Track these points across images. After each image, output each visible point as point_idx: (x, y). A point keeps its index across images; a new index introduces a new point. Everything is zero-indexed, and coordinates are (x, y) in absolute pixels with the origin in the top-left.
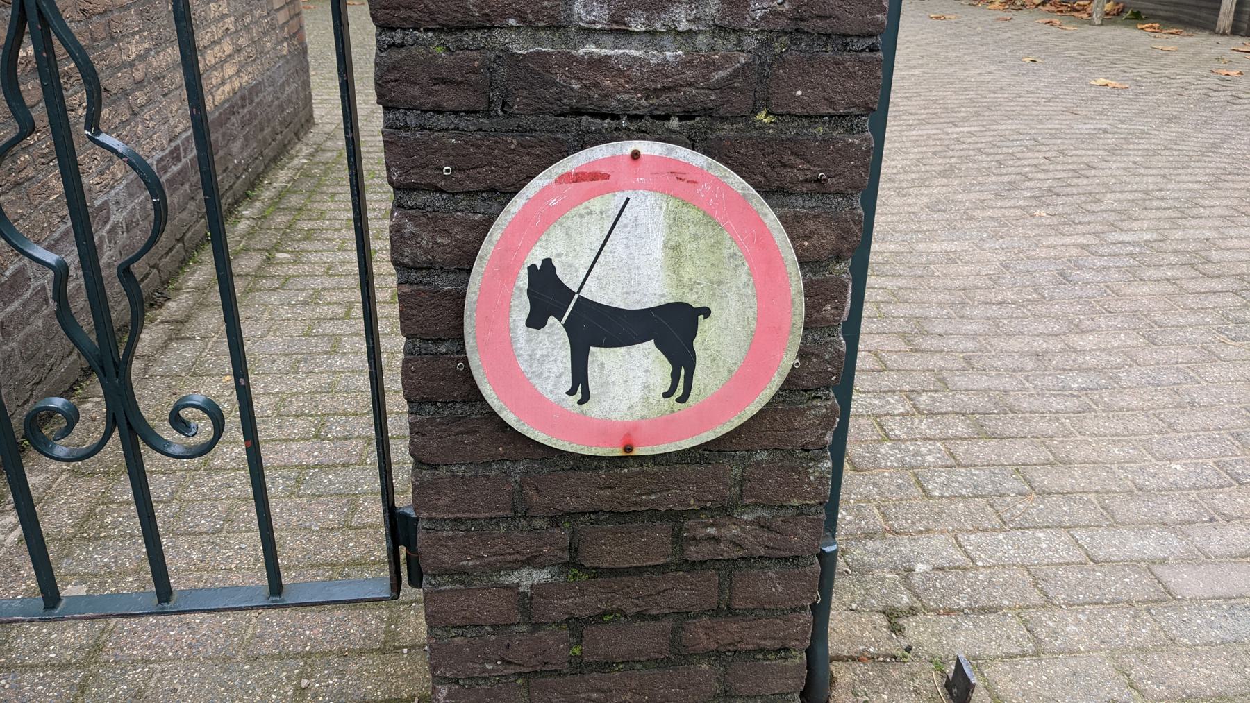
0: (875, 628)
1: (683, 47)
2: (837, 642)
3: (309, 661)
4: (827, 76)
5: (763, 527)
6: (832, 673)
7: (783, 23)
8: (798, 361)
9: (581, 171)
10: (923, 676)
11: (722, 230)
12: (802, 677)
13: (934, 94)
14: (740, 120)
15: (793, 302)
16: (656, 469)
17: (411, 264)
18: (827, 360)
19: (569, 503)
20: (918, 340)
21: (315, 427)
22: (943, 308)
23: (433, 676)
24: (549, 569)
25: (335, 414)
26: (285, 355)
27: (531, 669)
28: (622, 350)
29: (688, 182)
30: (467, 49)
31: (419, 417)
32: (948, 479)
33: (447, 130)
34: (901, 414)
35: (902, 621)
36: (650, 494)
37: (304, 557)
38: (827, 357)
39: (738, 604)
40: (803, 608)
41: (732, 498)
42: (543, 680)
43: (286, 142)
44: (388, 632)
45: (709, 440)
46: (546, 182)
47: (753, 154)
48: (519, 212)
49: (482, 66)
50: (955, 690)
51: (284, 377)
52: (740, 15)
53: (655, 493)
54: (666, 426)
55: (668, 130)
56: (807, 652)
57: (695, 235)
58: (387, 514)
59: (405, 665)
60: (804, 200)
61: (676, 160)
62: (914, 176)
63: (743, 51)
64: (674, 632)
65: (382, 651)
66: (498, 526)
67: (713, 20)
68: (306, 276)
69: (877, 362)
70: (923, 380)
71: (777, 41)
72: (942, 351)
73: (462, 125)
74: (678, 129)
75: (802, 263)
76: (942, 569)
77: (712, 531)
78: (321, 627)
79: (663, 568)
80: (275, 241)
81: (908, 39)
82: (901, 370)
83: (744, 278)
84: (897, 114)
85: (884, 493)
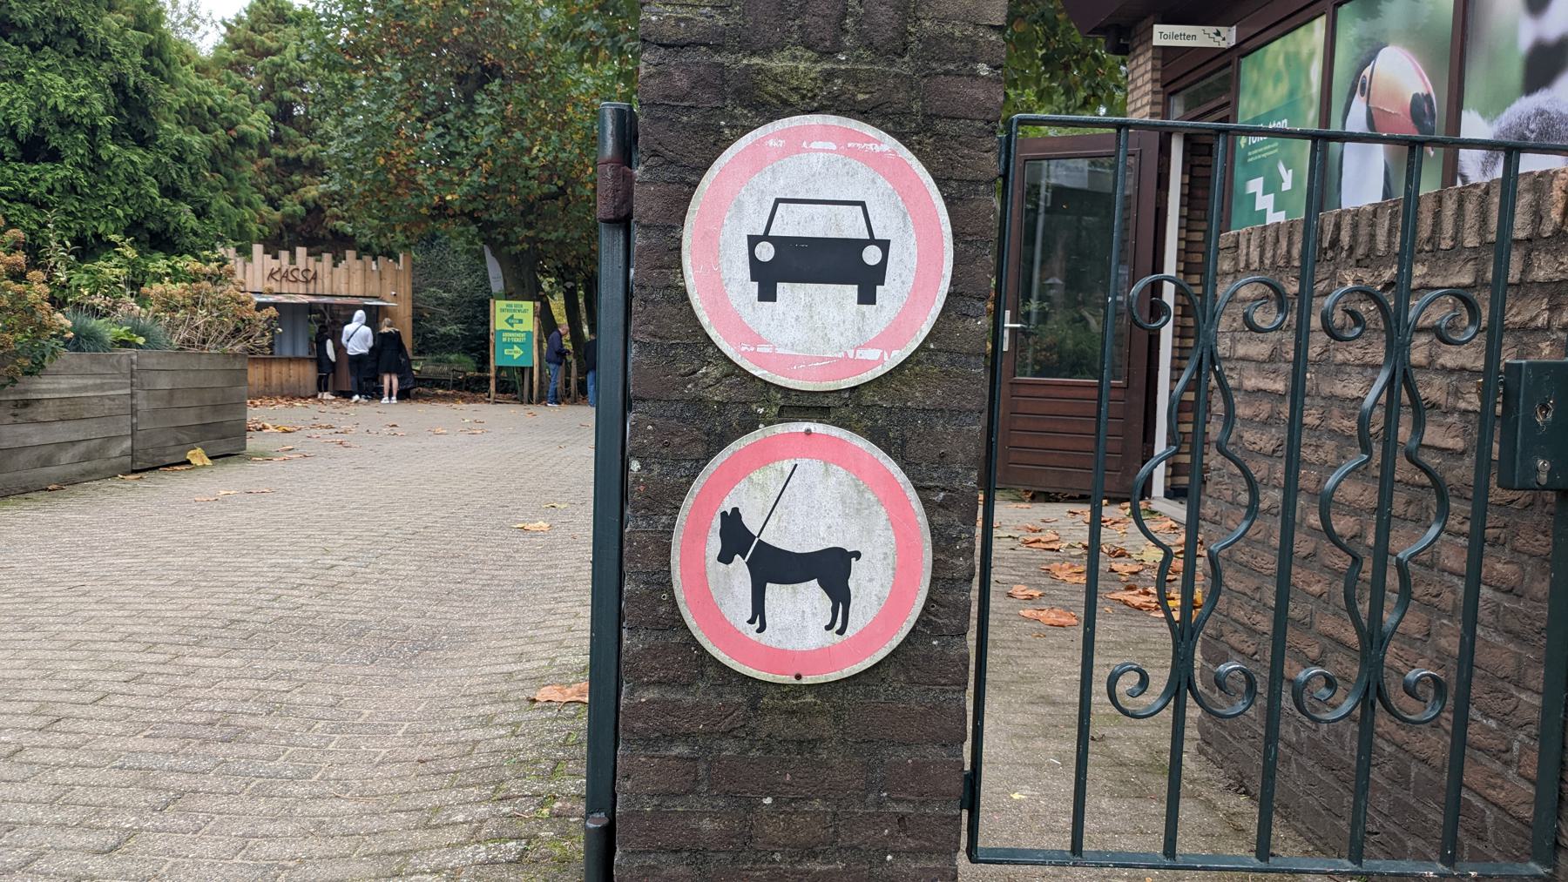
54: (823, 656)
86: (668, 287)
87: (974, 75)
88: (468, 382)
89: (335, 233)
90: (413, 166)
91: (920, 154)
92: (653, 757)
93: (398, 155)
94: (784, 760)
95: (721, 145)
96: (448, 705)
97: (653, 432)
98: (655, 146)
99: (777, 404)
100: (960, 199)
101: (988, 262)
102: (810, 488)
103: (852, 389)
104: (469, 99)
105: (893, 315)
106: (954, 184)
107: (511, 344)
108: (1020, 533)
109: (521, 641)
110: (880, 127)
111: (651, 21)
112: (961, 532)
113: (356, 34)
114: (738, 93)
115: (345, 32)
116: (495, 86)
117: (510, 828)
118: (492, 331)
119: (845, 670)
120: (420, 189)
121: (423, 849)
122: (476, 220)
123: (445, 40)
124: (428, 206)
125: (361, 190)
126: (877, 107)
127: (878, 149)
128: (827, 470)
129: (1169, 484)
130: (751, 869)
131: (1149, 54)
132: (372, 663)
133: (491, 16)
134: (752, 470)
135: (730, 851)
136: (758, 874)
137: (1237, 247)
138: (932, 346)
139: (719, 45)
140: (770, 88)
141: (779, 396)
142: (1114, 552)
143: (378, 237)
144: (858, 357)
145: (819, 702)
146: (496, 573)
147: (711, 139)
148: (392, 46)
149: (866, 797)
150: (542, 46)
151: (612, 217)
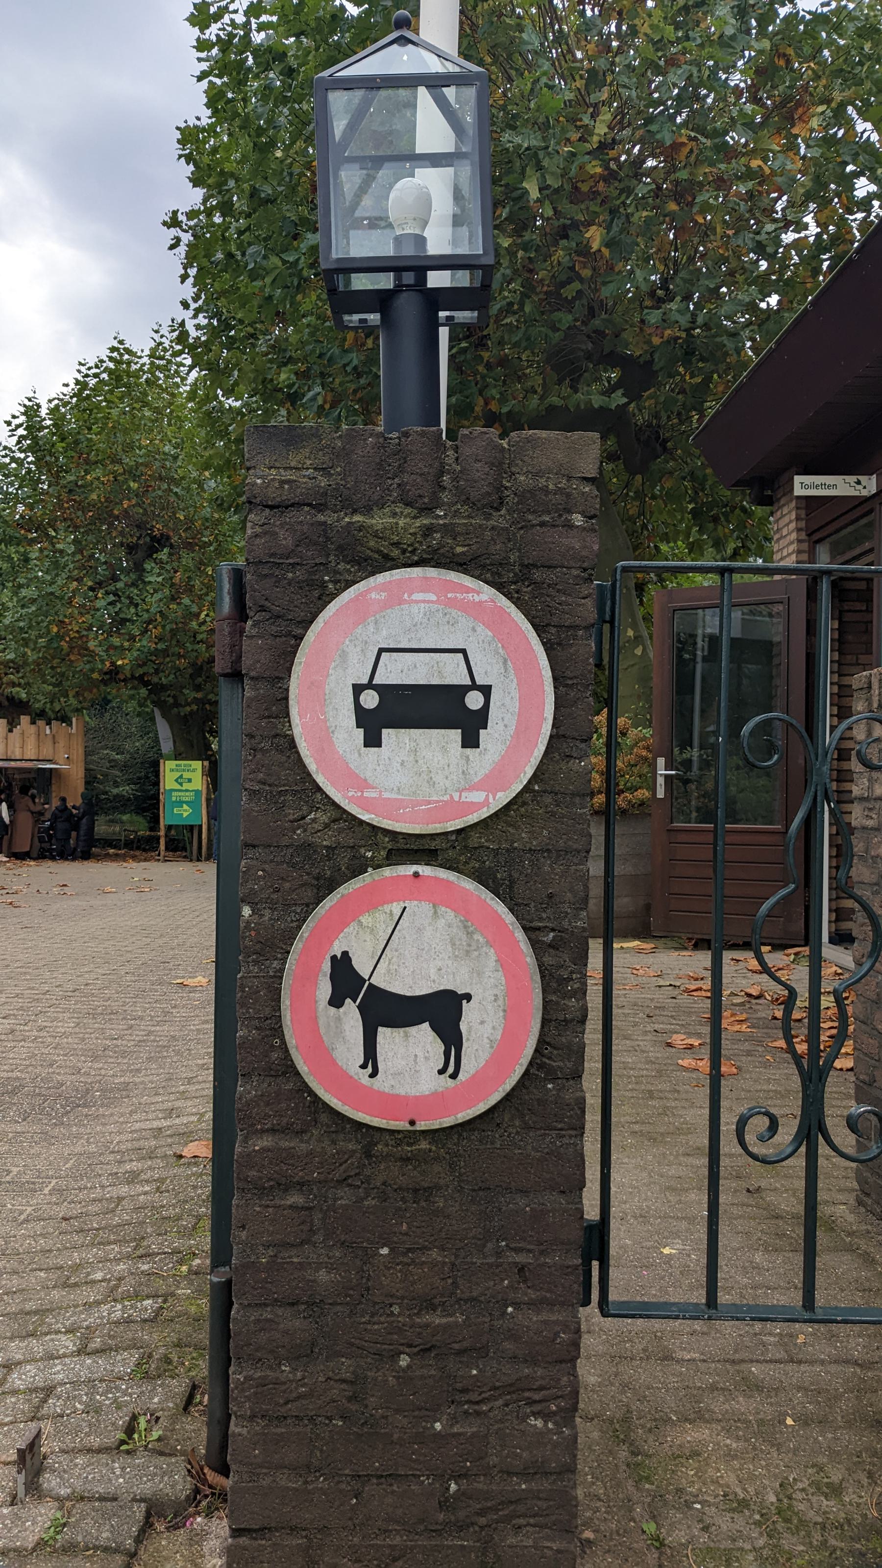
54: (437, 1100)
86: (277, 735)
87: (569, 526)
88: (139, 841)
89: (11, 699)
90: (85, 633)
91: (518, 603)
92: (268, 1206)
93: (70, 624)
94: (400, 1209)
95: (326, 598)
96: (96, 1161)
97: (264, 877)
98: (263, 602)
99: (384, 848)
100: (559, 644)
101: (589, 704)
102: (420, 930)
103: (459, 832)
104: (138, 568)
105: (497, 758)
106: (553, 630)
107: (180, 803)
108: (682, 981)
109: (172, 1097)
110: (478, 578)
111: (256, 484)
112: (572, 972)
113: (32, 510)
114: (341, 548)
115: (21, 508)
116: (164, 554)
117: (147, 1286)
118: (162, 790)
119: (459, 1116)
120: (92, 654)
121: (60, 1308)
122: (146, 684)
123: (116, 512)
124: (100, 672)
125: (35, 657)
126: (476, 558)
127: (477, 598)
128: (436, 912)
129: (833, 929)
130: (369, 1322)
131: (793, 504)
132: (24, 1120)
133: (159, 489)
134: (362, 913)
135: (347, 1304)
136: (376, 1327)
137: (870, 687)
138: (537, 788)
139: (321, 505)
140: (372, 544)
141: (387, 839)
142: (777, 999)
143: (52, 702)
144: (463, 799)
145: (434, 1148)
146: (153, 1029)
147: (316, 594)
148: (65, 520)
149: (484, 1246)
150: (208, 516)
151: (229, 671)
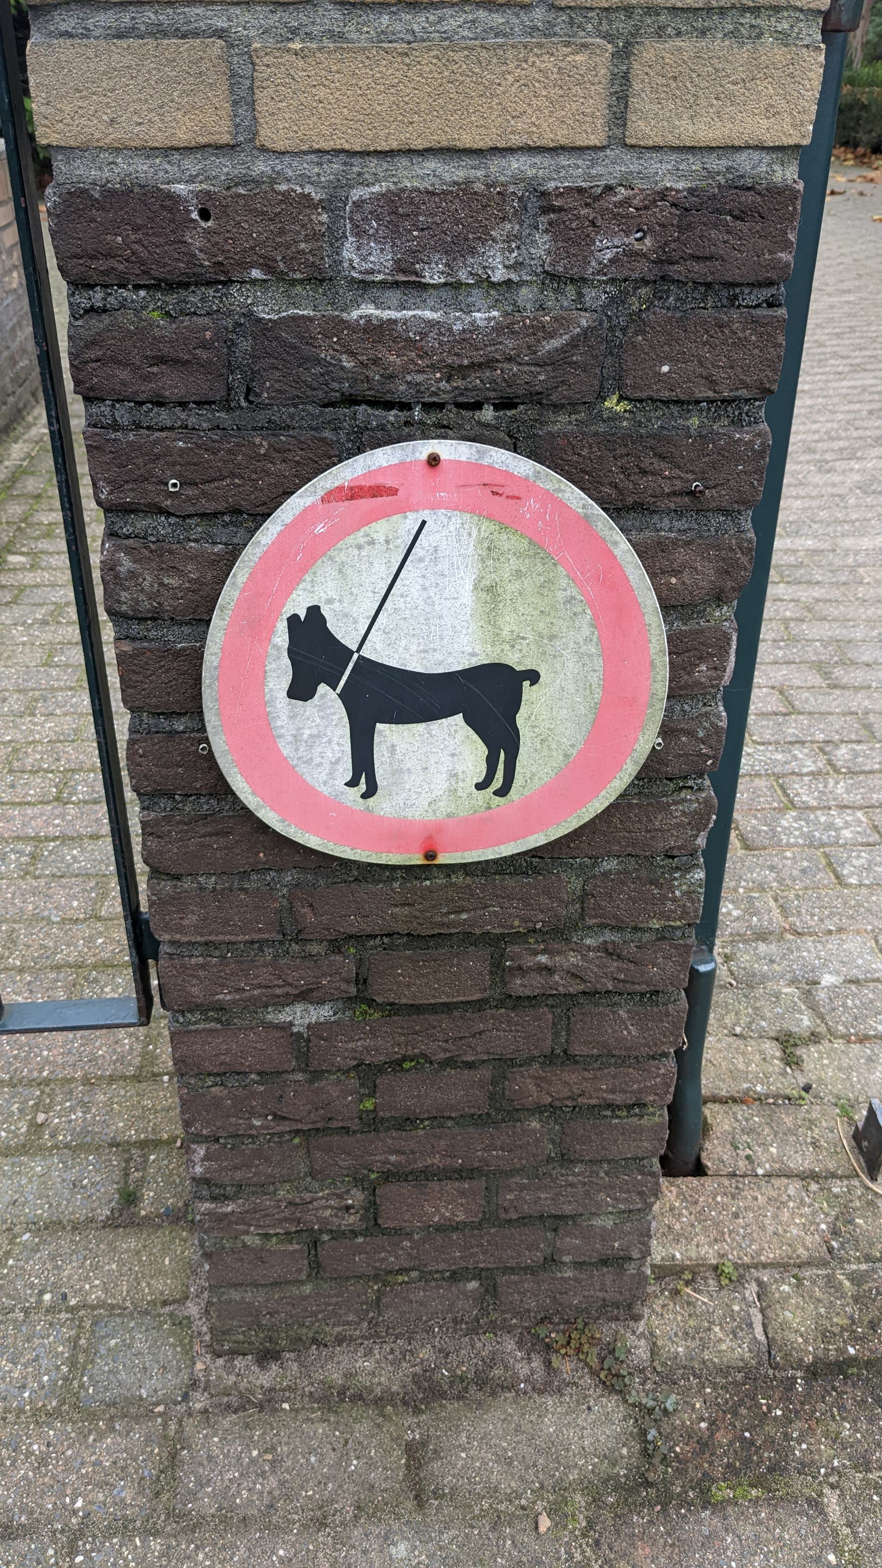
0: (764, 1059)
1: (499, 305)
2: (708, 1082)
3: (47, 1090)
4: (704, 344)
5: (611, 954)
6: (706, 1118)
7: (642, 269)
8: (660, 740)
9: (357, 484)
10: (824, 1124)
11: (555, 564)
12: (662, 1139)
13: (874, 328)
14: (582, 408)
15: (652, 664)
16: (468, 880)
17: (131, 613)
18: (701, 739)
19: (353, 924)
20: (838, 672)
21: (56, 786)
22: (873, 628)
23: (187, 1133)
24: (331, 1005)
25: (81, 770)
26: (19, 691)
27: (311, 1126)
28: (420, 727)
29: (507, 497)
30: (195, 313)
31: (153, 815)
32: (870, 862)
33: (172, 428)
34: (811, 773)
35: (801, 1051)
36: (461, 912)
37: (41, 957)
38: (701, 734)
39: (577, 1049)
40: (665, 1055)
41: (570, 918)
42: (328, 1139)
43: (21, 405)
44: (144, 1054)
45: (538, 845)
46: (309, 501)
47: (600, 457)
48: (273, 543)
49: (216, 337)
50: (865, 1144)
51: (18, 720)
52: (580, 258)
53: (468, 911)
55: (479, 423)
56: (669, 1107)
57: (518, 571)
58: (129, 921)
59: (165, 1096)
60: (671, 521)
61: (491, 467)
62: (841, 444)
63: (586, 310)
64: (494, 1082)
65: (137, 1078)
66: (263, 951)
67: (542, 266)
68: (45, 586)
69: (782, 701)
70: (843, 728)
71: (634, 294)
72: (869, 687)
73: (192, 421)
74: (494, 422)
75: (667, 607)
76: (856, 982)
77: (543, 959)
78: (61, 1047)
79: (480, 1005)
80: (6, 539)
81: (842, 251)
82: (814, 713)
83: (586, 631)
84: (822, 357)
85: (784, 880)
